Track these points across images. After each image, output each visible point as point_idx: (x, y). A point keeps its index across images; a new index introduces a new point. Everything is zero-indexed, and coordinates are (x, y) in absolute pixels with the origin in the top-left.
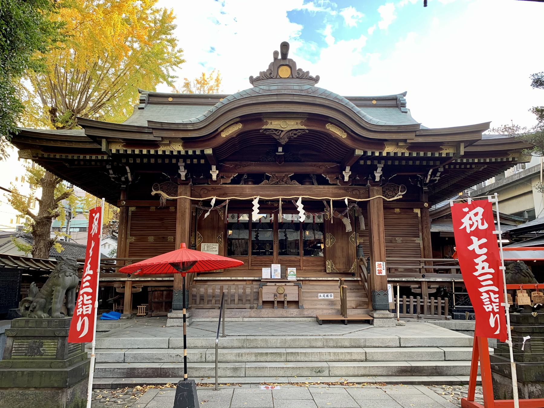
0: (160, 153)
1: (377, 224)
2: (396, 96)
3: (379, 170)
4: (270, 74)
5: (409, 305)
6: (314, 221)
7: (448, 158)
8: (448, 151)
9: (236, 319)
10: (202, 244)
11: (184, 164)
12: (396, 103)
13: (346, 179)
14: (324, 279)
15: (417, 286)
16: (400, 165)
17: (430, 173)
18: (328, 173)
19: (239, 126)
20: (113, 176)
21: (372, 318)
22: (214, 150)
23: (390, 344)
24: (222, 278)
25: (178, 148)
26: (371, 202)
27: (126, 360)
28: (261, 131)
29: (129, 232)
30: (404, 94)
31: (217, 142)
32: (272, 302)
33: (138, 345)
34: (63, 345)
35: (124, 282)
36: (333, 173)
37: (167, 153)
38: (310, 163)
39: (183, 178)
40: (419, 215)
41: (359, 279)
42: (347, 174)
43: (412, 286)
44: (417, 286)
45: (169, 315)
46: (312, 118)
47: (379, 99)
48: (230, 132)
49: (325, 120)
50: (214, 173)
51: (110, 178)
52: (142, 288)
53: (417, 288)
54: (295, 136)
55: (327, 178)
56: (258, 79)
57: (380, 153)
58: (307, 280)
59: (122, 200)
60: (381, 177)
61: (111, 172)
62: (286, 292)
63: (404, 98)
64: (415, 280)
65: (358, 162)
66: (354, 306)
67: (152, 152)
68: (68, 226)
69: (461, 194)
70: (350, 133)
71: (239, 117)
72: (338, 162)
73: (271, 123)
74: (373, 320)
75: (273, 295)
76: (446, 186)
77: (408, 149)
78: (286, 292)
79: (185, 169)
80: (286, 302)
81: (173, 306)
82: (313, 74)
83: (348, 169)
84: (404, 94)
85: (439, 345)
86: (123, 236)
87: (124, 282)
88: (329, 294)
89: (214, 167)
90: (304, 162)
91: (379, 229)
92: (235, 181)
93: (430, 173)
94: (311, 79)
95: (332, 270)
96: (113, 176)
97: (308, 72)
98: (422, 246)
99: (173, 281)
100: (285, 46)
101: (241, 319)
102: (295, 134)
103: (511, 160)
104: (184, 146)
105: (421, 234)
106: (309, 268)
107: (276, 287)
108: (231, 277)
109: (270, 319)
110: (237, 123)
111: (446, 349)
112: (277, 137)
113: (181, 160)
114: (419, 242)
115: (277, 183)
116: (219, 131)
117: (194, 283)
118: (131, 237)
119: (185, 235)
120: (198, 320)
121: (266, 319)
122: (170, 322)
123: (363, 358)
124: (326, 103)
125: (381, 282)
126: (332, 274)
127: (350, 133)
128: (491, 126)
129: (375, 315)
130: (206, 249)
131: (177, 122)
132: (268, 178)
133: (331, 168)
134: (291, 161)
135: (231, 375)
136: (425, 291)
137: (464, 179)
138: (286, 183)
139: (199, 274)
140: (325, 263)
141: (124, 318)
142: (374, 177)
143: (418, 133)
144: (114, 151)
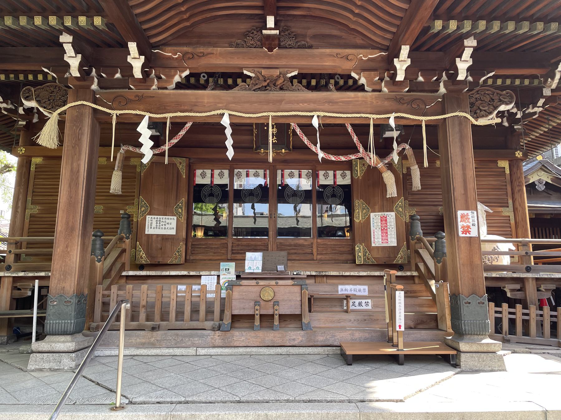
1: (460, 163)
3: (467, 53)
5: (501, 319)
6: (335, 182)
10: (148, 218)
14: (352, 274)
15: (518, 286)
18: (364, 68)
21: (454, 352)
26: (449, 124)
29: (29, 199)
41: (415, 274)
42: (402, 64)
44: (518, 286)
53: (519, 290)
58: (323, 276)
64: (515, 275)
69: (540, 158)
72: (382, 50)
75: (252, 304)
78: (278, 298)
80: (277, 317)
86: (20, 205)
88: (363, 301)
95: (364, 260)
98: (513, 222)
101: (192, 351)
105: (510, 201)
106: (327, 257)
107: (257, 289)
109: (248, 350)
114: (507, 214)
115: (264, 89)
118: (32, 207)
119: (77, 184)
120: (107, 352)
121: (241, 350)
122: (34, 362)
129: (463, 346)
130: (154, 225)
132: (246, 78)
133: (370, 60)
138: (281, 89)
139: (142, 267)
140: (353, 249)
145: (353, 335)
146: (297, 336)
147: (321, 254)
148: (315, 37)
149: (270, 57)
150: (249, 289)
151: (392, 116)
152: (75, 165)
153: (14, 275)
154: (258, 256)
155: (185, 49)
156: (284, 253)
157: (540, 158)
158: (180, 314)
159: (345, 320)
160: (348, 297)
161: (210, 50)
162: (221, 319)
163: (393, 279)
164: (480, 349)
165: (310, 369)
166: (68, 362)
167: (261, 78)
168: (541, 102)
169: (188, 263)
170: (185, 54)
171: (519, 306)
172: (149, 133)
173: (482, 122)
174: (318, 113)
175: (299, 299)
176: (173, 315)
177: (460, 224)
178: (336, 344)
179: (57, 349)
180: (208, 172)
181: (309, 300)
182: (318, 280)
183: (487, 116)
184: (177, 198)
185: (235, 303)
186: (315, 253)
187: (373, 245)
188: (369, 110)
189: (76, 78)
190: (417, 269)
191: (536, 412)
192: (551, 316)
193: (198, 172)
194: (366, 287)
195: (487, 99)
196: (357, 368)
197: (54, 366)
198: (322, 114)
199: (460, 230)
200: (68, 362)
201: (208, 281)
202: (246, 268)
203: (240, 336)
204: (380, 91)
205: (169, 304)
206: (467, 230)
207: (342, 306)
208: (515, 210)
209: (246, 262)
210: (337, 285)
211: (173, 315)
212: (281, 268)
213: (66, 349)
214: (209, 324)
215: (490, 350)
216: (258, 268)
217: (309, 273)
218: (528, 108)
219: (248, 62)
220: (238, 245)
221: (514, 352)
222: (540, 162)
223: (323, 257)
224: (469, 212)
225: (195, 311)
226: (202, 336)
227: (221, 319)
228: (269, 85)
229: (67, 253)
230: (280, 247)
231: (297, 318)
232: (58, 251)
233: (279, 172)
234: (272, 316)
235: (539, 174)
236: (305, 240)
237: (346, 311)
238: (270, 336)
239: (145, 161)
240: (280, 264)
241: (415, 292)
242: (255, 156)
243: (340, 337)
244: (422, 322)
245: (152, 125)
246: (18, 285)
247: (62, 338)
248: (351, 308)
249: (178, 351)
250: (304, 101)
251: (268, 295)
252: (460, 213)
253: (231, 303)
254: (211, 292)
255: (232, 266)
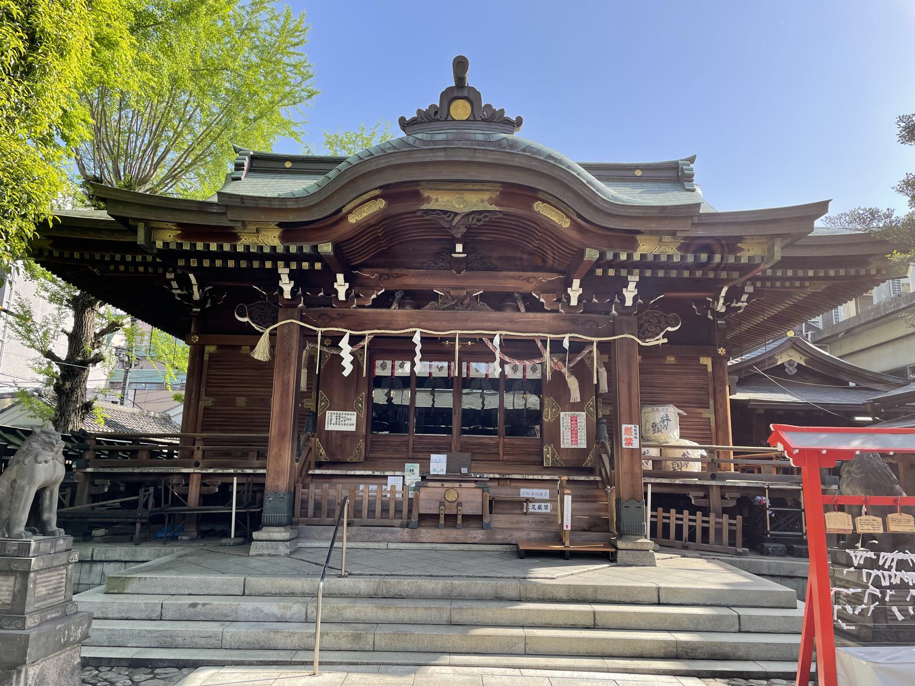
0: (240, 249)
1: (288, 614)
2: (677, 163)
3: (632, 286)
4: (436, 113)
7: (751, 266)
8: (751, 253)
9: (376, 545)
10: (328, 413)
11: (287, 271)
12: (676, 175)
13: (574, 302)
14: (536, 477)
16: (679, 279)
17: (723, 293)
18: (544, 291)
19: (381, 204)
20: (179, 291)
21: (614, 550)
22: (337, 247)
23: (641, 598)
24: (358, 473)
25: (271, 239)
27: (164, 614)
28: (418, 214)
29: (203, 390)
30: (692, 160)
31: (341, 231)
32: (436, 517)
33: (189, 589)
34: (25, 588)
35: (188, 474)
36: (552, 291)
37: (252, 250)
38: (511, 273)
39: (287, 295)
40: (710, 369)
41: (598, 478)
42: (575, 291)
43: (692, 495)
44: (702, 494)
45: (255, 535)
46: (510, 192)
47: (645, 168)
48: (365, 215)
49: (532, 194)
50: (341, 287)
51: (173, 295)
52: (220, 487)
53: (702, 498)
54: (479, 224)
55: (542, 300)
56: (414, 122)
57: (630, 256)
59: (194, 334)
60: (635, 299)
61: (174, 284)
62: (460, 499)
63: (692, 166)
65: (591, 271)
66: (586, 527)
67: (227, 247)
68: (125, 379)
69: (791, 334)
70: (575, 218)
71: (380, 188)
72: (560, 272)
73: (437, 200)
74: (616, 552)
75: (438, 504)
76: (759, 319)
77: (679, 249)
79: (290, 280)
80: (460, 517)
81: (265, 519)
82: (511, 115)
83: (576, 283)
84: (692, 160)
85: (731, 604)
86: (193, 396)
87: (187, 475)
88: (543, 504)
89: (340, 277)
90: (501, 270)
91: (630, 391)
92: (380, 303)
93: (723, 293)
94: (508, 122)
95: (553, 462)
96: (179, 291)
97: (502, 111)
98: (713, 424)
99: (264, 475)
100: (461, 65)
101: (383, 545)
102: (479, 220)
103: (873, 272)
104: (284, 238)
105: (711, 402)
107: (443, 490)
108: (374, 470)
109: (434, 545)
110: (375, 198)
111: (742, 612)
112: (446, 225)
113: (281, 264)
115: (452, 308)
116: (344, 211)
117: (309, 479)
119: (287, 395)
120: (308, 544)
121: (427, 546)
122: (255, 548)
123: (590, 622)
124: (533, 165)
125: (633, 486)
126: (553, 469)
127: (575, 218)
128: (832, 211)
129: (620, 544)
130: (334, 421)
131: (269, 195)
134: (478, 270)
135: (349, 646)
136: (715, 500)
137: (791, 306)
139: (319, 465)
141: (185, 538)
142: (623, 299)
143: (696, 220)
144: (159, 245)
145: (529, 534)
146: (478, 534)
147: (508, 455)
148: (500, 258)
149: (458, 278)
150: (433, 491)
151: (567, 336)
152: (285, 377)
153: (204, 471)
154: (443, 458)
155: (382, 270)
156: (468, 455)
157: (791, 334)
158: (371, 512)
159: (522, 522)
160: (527, 500)
161: (404, 271)
162: (409, 518)
163: (565, 483)
164: (634, 547)
165: (488, 560)
166: (283, 549)
167: (450, 298)
168: (745, 297)
169: (367, 462)
170: (381, 275)
171: (699, 514)
172: (349, 348)
173: (651, 342)
174: (501, 332)
175: (480, 501)
176: (365, 512)
177: (624, 437)
178: (513, 542)
179: (273, 538)
180: (389, 363)
181: (491, 502)
182: (502, 482)
183: (654, 337)
184: (357, 392)
185: (421, 503)
186: (501, 455)
187: (562, 446)
188: (546, 330)
189: (287, 299)
190: (601, 475)
191: (651, 588)
192: (730, 524)
193: (378, 363)
194: (548, 491)
195: (654, 321)
196: (526, 561)
197: (272, 552)
198: (504, 333)
199: (624, 442)
200: (283, 549)
201: (394, 481)
202: (431, 470)
203: (426, 533)
204: (557, 311)
205: (361, 502)
206: (629, 442)
207: (522, 508)
208: (716, 412)
209: (431, 464)
210: (519, 488)
211: (365, 512)
212: (464, 470)
213: (281, 538)
214: (398, 522)
215: (643, 548)
216: (442, 470)
217: (492, 476)
218: (732, 302)
219: (438, 283)
220: (420, 443)
221: (684, 556)
222: (790, 339)
223: (510, 458)
224: (632, 426)
225: (385, 510)
226: (393, 532)
227: (409, 518)
228: (458, 303)
229: (279, 456)
230: (464, 448)
231: (479, 518)
232: (272, 452)
233: (464, 364)
234: (456, 516)
235: (790, 354)
236: (491, 439)
237: (526, 514)
238: (454, 534)
239: (346, 373)
240: (464, 467)
241: (595, 496)
242: (439, 348)
243: (517, 536)
244: (595, 525)
245: (354, 341)
246: (207, 481)
247: (277, 529)
248: (531, 510)
249: (371, 545)
250: (489, 321)
251: (452, 496)
252: (624, 426)
253: (418, 504)
254: (399, 492)
255: (416, 467)
